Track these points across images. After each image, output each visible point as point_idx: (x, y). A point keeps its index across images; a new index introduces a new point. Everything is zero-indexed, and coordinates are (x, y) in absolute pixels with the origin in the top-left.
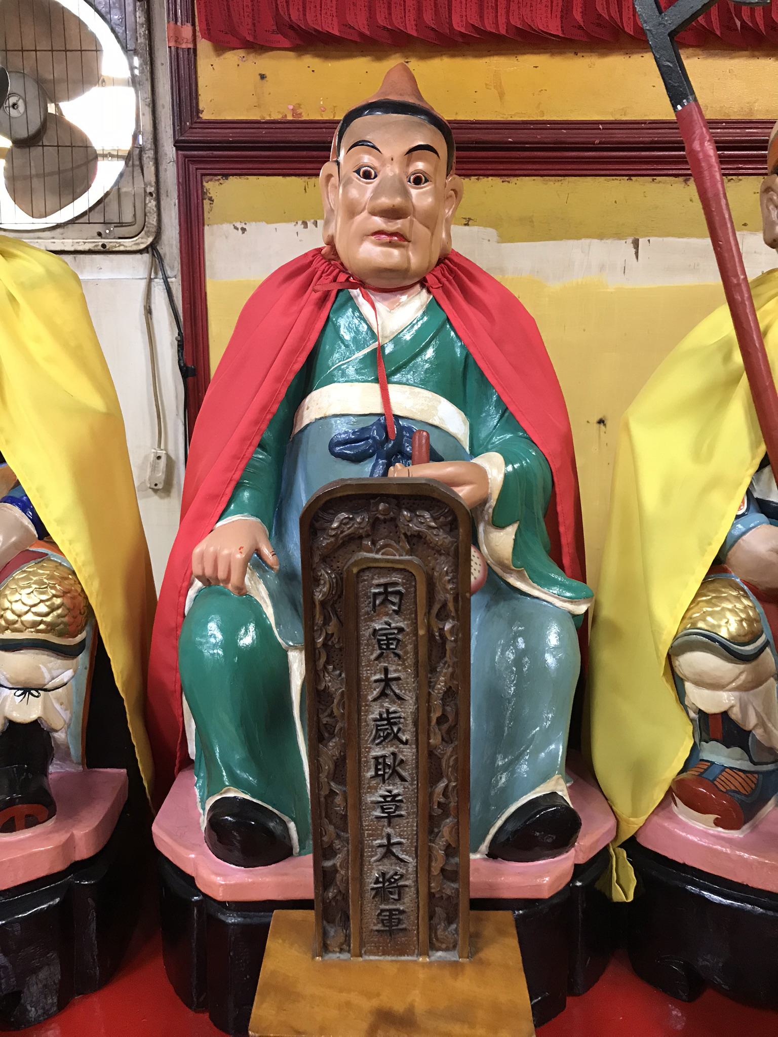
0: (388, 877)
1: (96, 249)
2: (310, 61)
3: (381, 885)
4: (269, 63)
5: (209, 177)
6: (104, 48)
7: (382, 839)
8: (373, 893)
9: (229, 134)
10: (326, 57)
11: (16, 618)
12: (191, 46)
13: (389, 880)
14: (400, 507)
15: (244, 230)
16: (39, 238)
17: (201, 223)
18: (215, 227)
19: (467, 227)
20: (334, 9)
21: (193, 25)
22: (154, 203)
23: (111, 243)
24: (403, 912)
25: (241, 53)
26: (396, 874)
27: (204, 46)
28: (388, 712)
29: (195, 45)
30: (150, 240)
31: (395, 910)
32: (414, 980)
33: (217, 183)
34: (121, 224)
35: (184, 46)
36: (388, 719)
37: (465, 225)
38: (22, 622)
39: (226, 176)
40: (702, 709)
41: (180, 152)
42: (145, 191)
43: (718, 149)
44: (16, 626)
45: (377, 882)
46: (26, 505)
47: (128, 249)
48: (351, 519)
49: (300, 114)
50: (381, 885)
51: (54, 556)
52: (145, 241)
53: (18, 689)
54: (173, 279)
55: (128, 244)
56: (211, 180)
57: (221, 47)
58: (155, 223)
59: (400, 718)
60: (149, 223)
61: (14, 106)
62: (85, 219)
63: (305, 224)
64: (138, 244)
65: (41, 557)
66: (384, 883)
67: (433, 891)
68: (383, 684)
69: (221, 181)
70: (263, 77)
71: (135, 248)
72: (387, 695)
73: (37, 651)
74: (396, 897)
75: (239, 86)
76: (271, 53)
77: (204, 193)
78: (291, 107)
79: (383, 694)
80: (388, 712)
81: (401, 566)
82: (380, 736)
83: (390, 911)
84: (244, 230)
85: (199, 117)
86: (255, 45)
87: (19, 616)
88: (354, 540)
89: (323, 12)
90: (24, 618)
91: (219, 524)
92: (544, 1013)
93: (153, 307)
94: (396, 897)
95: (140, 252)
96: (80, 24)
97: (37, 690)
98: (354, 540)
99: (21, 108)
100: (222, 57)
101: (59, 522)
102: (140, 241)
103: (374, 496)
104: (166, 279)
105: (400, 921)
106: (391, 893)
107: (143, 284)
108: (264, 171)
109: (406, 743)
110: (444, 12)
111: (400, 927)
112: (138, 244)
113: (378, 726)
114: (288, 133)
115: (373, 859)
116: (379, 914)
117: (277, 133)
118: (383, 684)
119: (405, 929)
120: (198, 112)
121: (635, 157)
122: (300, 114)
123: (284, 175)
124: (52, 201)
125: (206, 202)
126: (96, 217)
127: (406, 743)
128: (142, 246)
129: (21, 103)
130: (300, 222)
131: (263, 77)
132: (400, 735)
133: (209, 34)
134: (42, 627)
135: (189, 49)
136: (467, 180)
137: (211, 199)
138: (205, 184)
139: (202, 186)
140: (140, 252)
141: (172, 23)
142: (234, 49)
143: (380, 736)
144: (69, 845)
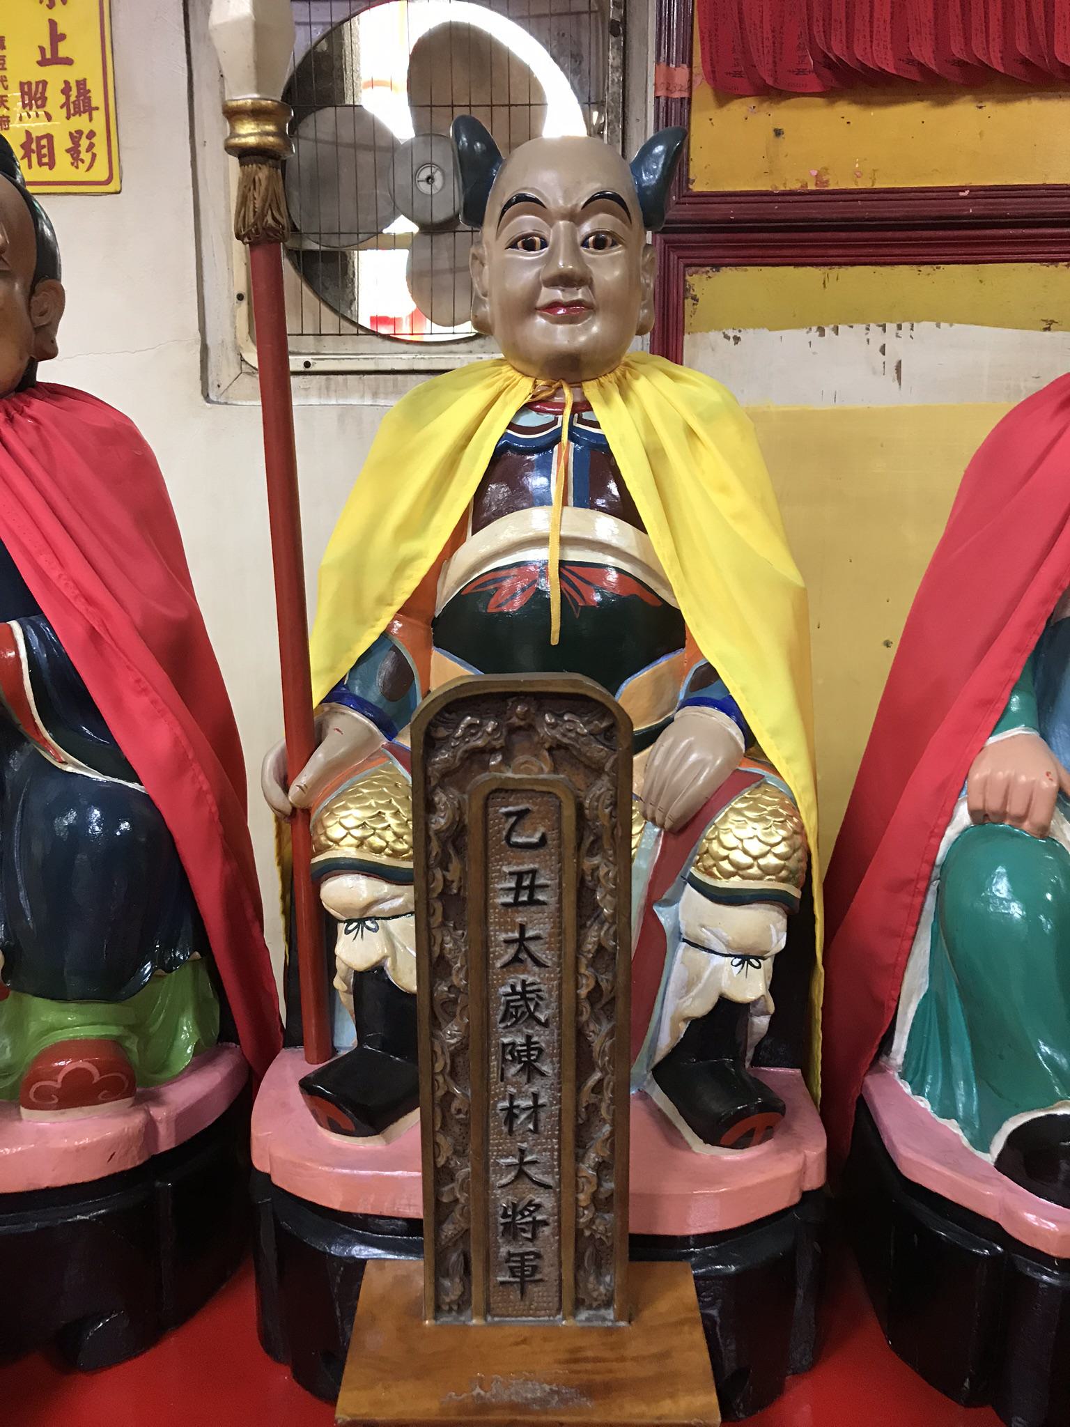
2: (845, 110)
3: (509, 1220)
4: (787, 114)
5: (693, 269)
6: (549, 100)
9: (731, 211)
10: (867, 103)
11: (749, 860)
12: (686, 95)
14: (541, 711)
16: (451, 352)
17: (680, 332)
19: (1047, 333)
20: (889, 39)
21: (690, 66)
24: (538, 1256)
25: (751, 101)
26: (530, 1204)
27: (703, 93)
28: (524, 982)
29: (691, 94)
32: (521, 1347)
33: (705, 276)
35: (677, 95)
36: (524, 992)
37: (1045, 329)
38: (759, 866)
39: (717, 267)
40: (67, 67)
41: (658, 237)
43: (78, 83)
44: (750, 871)
45: (505, 1215)
46: (728, 706)
48: (480, 725)
49: (827, 182)
50: (509, 1220)
51: (771, 779)
53: (736, 956)
56: (696, 273)
57: (725, 94)
59: (539, 990)
63: (821, 331)
65: (755, 781)
67: (581, 1226)
68: (516, 946)
70: (778, 133)
72: (521, 961)
73: (768, 906)
75: (748, 148)
76: (793, 100)
77: (686, 290)
78: (815, 173)
79: (516, 959)
81: (544, 789)
82: (512, 1016)
83: (522, 1255)
84: (737, 339)
85: (689, 189)
86: (771, 91)
87: (755, 858)
88: (477, 757)
89: (875, 42)
90: (762, 862)
91: (992, 740)
94: (529, 1236)
96: (526, 73)
97: (757, 958)
98: (477, 757)
100: (724, 110)
101: (774, 733)
105: (535, 1269)
106: (524, 1231)
109: (545, 1025)
110: (1042, 40)
111: (538, 1277)
113: (508, 1002)
114: (922, 206)
116: (508, 1261)
117: (934, 206)
118: (516, 946)
119: (541, 1280)
120: (688, 181)
121: (1011, 237)
122: (827, 182)
123: (797, 265)
125: (688, 302)
127: (545, 1025)
130: (814, 329)
131: (778, 133)
132: (537, 1014)
133: (714, 79)
134: (784, 873)
135: (682, 99)
136: (1052, 267)
137: (695, 299)
138: (688, 277)
139: (685, 281)
141: (663, 65)
142: (741, 97)
144: (803, 1171)
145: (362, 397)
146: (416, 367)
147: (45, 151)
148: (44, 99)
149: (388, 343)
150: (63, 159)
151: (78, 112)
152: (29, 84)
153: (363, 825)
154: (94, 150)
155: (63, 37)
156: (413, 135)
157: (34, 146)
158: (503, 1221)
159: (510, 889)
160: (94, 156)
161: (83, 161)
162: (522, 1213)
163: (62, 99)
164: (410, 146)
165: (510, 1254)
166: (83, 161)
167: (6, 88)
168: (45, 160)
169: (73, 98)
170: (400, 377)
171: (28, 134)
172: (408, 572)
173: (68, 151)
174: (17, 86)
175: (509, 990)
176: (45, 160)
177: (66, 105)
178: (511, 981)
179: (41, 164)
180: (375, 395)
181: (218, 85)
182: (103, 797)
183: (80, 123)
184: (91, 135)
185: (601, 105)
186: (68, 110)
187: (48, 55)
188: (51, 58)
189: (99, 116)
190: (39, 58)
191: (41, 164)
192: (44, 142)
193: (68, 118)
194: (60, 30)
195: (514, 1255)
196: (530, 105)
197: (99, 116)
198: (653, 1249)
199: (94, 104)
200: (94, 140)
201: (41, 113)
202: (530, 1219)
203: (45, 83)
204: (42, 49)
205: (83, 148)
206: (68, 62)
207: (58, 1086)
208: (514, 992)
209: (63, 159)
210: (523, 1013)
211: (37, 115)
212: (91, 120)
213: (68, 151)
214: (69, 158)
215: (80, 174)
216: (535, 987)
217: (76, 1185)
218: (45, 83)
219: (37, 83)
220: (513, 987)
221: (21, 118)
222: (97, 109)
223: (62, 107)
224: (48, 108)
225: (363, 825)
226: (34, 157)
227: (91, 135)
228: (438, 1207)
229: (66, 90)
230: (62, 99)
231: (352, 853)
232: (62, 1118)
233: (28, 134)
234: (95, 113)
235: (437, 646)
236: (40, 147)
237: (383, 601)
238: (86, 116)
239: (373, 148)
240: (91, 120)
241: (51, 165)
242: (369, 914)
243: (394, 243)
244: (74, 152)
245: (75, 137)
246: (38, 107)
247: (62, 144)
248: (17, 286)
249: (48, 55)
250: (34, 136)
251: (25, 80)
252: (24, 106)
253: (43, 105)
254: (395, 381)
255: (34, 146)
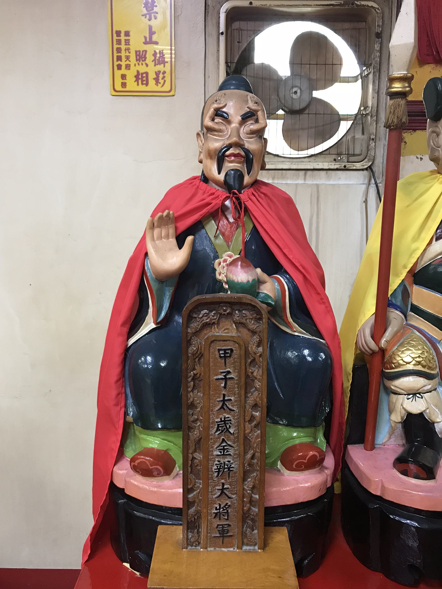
0: (222, 506)
1: (341, 168)
5: (405, 131)
7: (219, 486)
8: (214, 515)
13: (222, 508)
15: (421, 159)
18: (406, 157)
22: (374, 144)
23: (349, 165)
25: (433, 66)
30: (370, 163)
31: (226, 525)
33: (410, 134)
34: (354, 155)
36: (224, 421)
39: (415, 130)
42: (370, 138)
47: (358, 168)
52: (366, 164)
54: (381, 185)
55: (358, 165)
56: (406, 132)
58: (373, 155)
59: (230, 420)
60: (370, 154)
61: (296, 92)
62: (327, 152)
64: (364, 166)
66: (219, 509)
68: (220, 491)
69: (412, 133)
71: (361, 168)
72: (224, 409)
74: (226, 518)
79: (222, 407)
80: (225, 418)
82: (220, 430)
83: (222, 525)
84: (421, 159)
92: (301, 571)
93: (368, 199)
94: (226, 518)
95: (363, 170)
98: (207, 325)
99: (299, 94)
102: (365, 164)
103: (221, 303)
104: (376, 183)
107: (364, 187)
108: (421, 128)
112: (364, 166)
115: (214, 497)
116: (217, 527)
124: (311, 142)
125: (403, 144)
126: (333, 151)
128: (366, 167)
129: (299, 91)
137: (405, 142)
138: (403, 134)
140: (363, 170)
142: (429, 63)
143: (220, 430)
145: (268, 179)
146: (292, 168)
147: (144, 79)
148: (145, 58)
149: (276, 157)
150: (152, 82)
151: (159, 63)
152: (139, 51)
153: (419, 357)
154: (165, 79)
155: (154, 33)
156: (289, 75)
157: (140, 77)
158: (217, 522)
159: (222, 379)
160: (165, 81)
161: (160, 83)
162: (222, 508)
163: (153, 58)
164: (287, 79)
165: (218, 525)
166: (160, 83)
167: (130, 53)
168: (145, 82)
169: (157, 58)
170: (284, 172)
171: (138, 72)
172: (413, 255)
173: (154, 79)
174: (134, 53)
175: (219, 420)
176: (145, 82)
177: (154, 60)
178: (221, 416)
179: (142, 84)
180: (273, 178)
181: (216, 54)
182: (309, 344)
183: (160, 68)
184: (164, 73)
185: (368, 66)
186: (155, 63)
187: (148, 40)
188: (149, 41)
189: (168, 65)
190: (144, 41)
191: (142, 84)
192: (144, 75)
193: (155, 66)
194: (153, 30)
195: (220, 525)
196: (333, 64)
197: (168, 65)
198: (273, 516)
199: (166, 60)
200: (165, 75)
201: (144, 63)
202: (226, 511)
203: (146, 51)
204: (145, 38)
205: (160, 78)
206: (156, 43)
207: (306, 461)
208: (221, 421)
209: (152, 82)
210: (224, 429)
211: (142, 64)
212: (164, 66)
213: (154, 79)
214: (154, 82)
215: (159, 88)
216: (228, 419)
217: (310, 501)
218: (146, 51)
219: (143, 51)
220: (221, 419)
221: (135, 65)
222: (167, 62)
223: (153, 61)
224: (147, 62)
225: (419, 357)
226: (140, 81)
227: (164, 73)
228: (188, 503)
229: (155, 54)
230: (153, 58)
231: (410, 367)
232: (301, 474)
233: (138, 72)
234: (166, 64)
235: (416, 284)
236: (142, 77)
237: (405, 267)
238: (162, 65)
239: (270, 79)
240: (164, 66)
241: (147, 84)
242: (419, 392)
243: (277, 118)
244: (157, 80)
245: (157, 73)
246: (143, 61)
247: (152, 76)
248: (235, 139)
249: (148, 40)
250: (140, 73)
251: (138, 50)
252: (137, 60)
253: (145, 60)
254: (282, 174)
255: (140, 77)
